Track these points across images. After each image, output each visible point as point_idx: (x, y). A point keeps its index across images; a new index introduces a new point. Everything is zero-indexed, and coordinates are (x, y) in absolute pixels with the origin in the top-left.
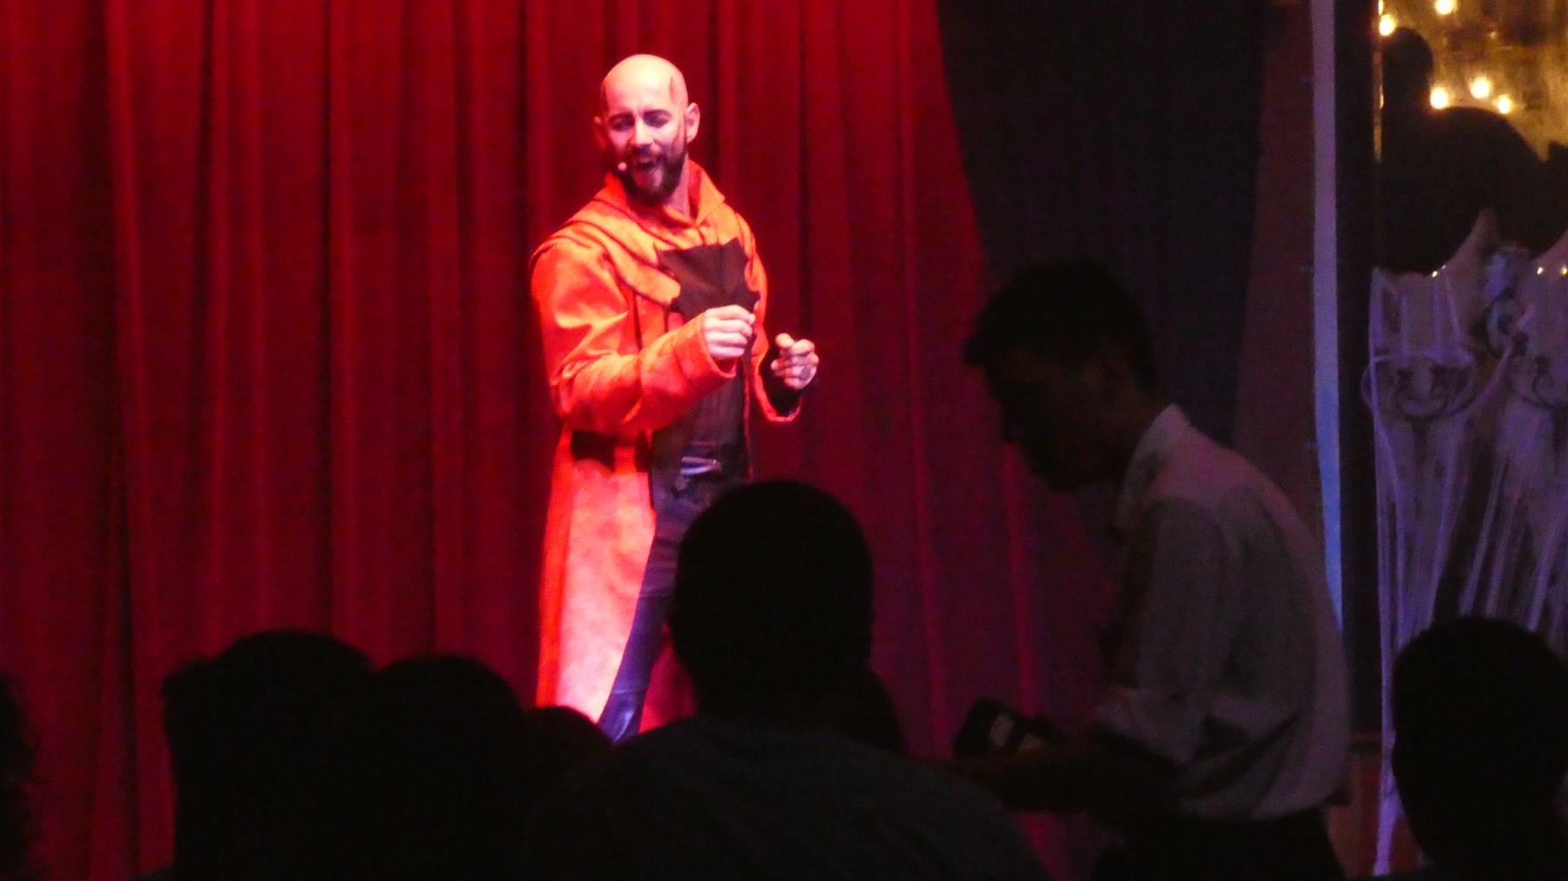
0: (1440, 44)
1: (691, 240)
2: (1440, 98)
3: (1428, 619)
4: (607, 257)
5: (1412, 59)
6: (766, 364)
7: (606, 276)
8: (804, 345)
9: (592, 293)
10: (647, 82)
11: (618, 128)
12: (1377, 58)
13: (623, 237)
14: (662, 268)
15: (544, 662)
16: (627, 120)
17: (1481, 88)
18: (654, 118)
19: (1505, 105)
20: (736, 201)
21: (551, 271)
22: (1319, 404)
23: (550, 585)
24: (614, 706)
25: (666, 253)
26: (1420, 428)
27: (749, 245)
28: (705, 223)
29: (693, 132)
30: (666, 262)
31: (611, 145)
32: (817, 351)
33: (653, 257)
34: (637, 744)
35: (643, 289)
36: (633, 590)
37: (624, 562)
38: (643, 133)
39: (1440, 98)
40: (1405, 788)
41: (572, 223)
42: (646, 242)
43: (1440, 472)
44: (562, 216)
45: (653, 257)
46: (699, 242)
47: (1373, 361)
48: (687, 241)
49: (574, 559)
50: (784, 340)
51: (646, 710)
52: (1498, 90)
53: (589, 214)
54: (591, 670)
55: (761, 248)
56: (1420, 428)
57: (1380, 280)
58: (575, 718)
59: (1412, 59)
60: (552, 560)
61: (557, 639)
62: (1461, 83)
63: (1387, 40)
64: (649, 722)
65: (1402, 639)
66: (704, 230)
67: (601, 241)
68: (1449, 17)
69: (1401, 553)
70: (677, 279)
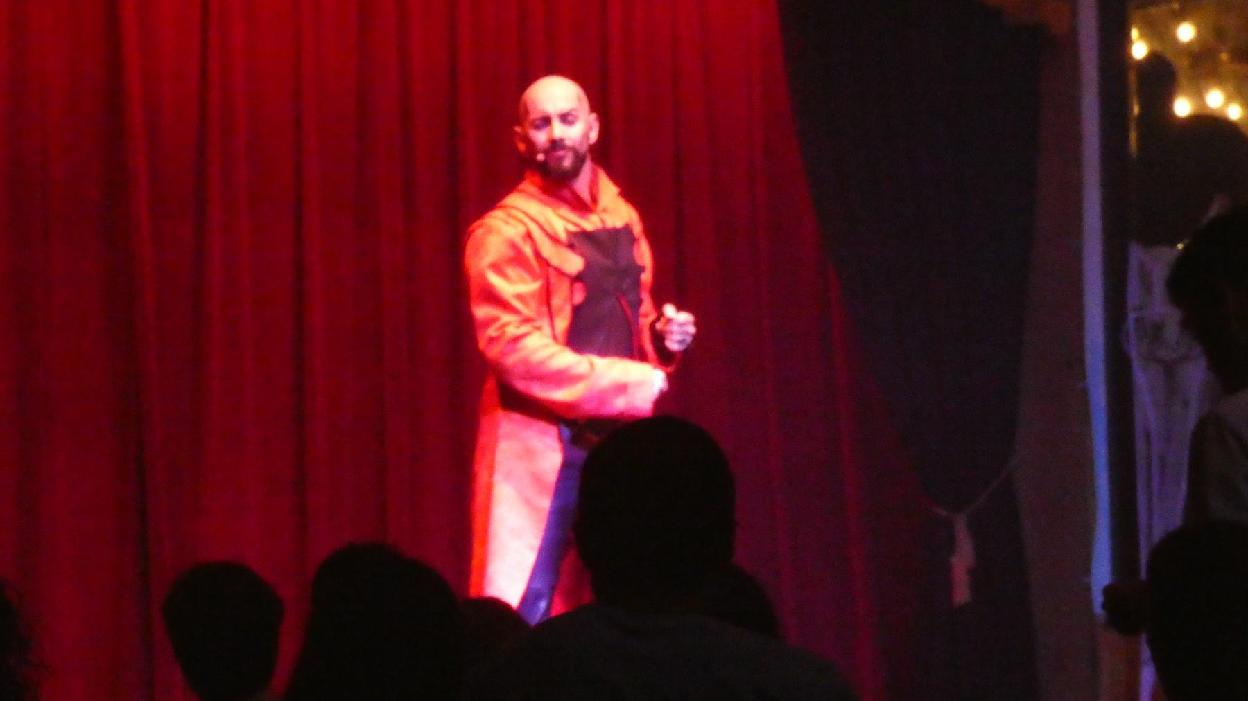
0: (1181, 64)
1: (592, 223)
2: (1182, 107)
3: (1176, 518)
4: (529, 236)
5: (1161, 76)
6: (652, 326)
7: (528, 250)
8: (685, 317)
9: (517, 258)
10: (556, 95)
11: (538, 127)
12: (1132, 78)
13: (541, 219)
14: (571, 246)
15: (475, 562)
16: (546, 121)
17: (1215, 99)
18: (566, 118)
19: (1234, 112)
20: (628, 194)
21: (480, 246)
22: (1088, 356)
23: (479, 499)
24: (530, 597)
25: (576, 234)
26: (1170, 370)
27: (637, 229)
28: (604, 211)
29: (594, 136)
30: (575, 241)
31: (530, 143)
32: (696, 324)
33: (563, 236)
34: (549, 624)
35: (555, 262)
36: (545, 503)
37: (537, 479)
38: (558, 130)
39: (1182, 107)
40: (1158, 660)
41: (501, 207)
42: (560, 221)
43: (1186, 404)
44: (491, 199)
45: (563, 236)
46: (599, 225)
47: (1132, 316)
48: (591, 223)
49: (498, 479)
50: (669, 310)
51: (557, 600)
52: (1229, 99)
53: (514, 200)
54: (511, 562)
55: (649, 232)
56: (1170, 370)
57: (1137, 253)
58: (498, 605)
59: (1161, 76)
60: (482, 477)
61: (485, 540)
62: (1199, 95)
63: (1139, 63)
64: (559, 609)
65: (1158, 533)
66: (605, 216)
67: (521, 224)
68: (1189, 44)
69: (1155, 470)
70: (582, 255)
